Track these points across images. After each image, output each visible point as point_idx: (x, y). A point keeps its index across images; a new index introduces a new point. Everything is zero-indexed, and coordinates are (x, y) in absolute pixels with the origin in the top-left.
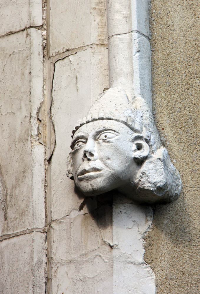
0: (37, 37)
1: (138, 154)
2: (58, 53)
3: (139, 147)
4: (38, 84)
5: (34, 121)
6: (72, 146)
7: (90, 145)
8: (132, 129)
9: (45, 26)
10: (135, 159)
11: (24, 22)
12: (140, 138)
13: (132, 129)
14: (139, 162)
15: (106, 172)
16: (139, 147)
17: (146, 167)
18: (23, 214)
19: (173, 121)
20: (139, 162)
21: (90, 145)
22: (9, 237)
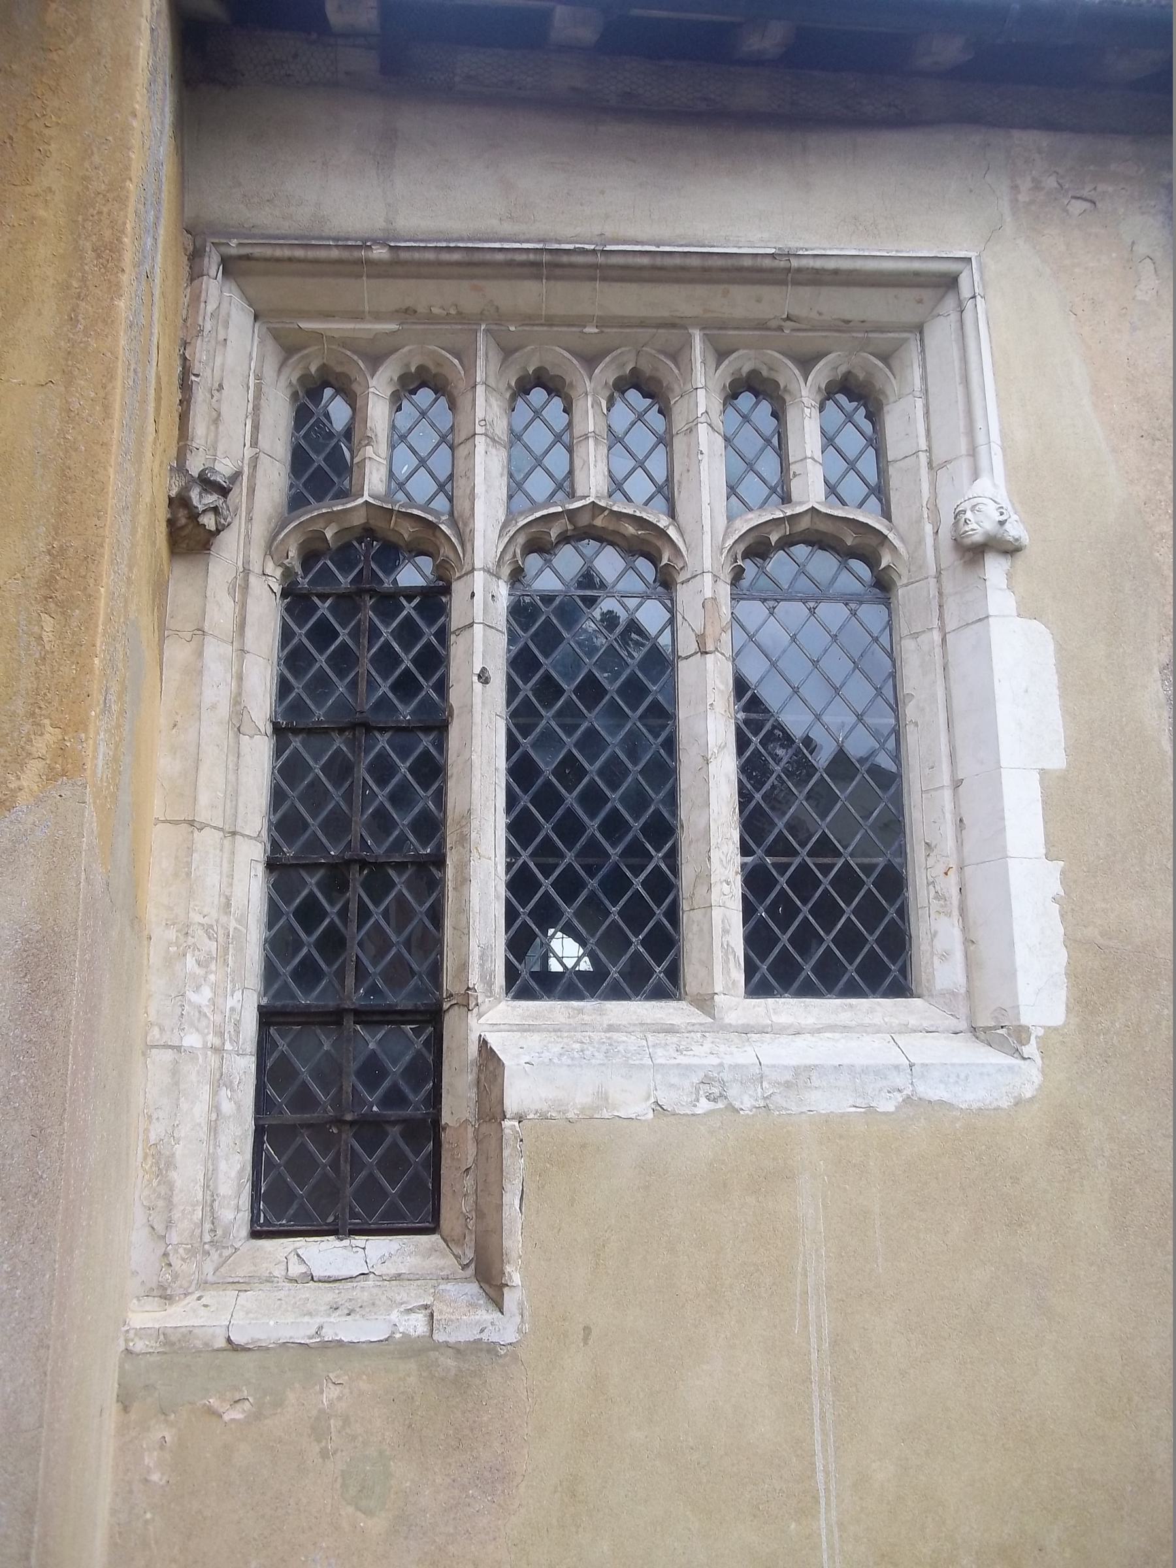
0: (923, 458)
1: (1002, 518)
2: (939, 465)
3: (1002, 514)
4: (925, 487)
5: (925, 509)
6: (955, 518)
7: (969, 515)
8: (995, 502)
9: (929, 450)
10: (1000, 522)
11: (336, 1541)
12: (1002, 508)
13: (995, 502)
14: (1002, 523)
15: (980, 530)
16: (1002, 514)
17: (1007, 526)
18: (920, 567)
19: (207, 1238)
20: (1002, 523)
21: (969, 515)
22: (913, 583)
